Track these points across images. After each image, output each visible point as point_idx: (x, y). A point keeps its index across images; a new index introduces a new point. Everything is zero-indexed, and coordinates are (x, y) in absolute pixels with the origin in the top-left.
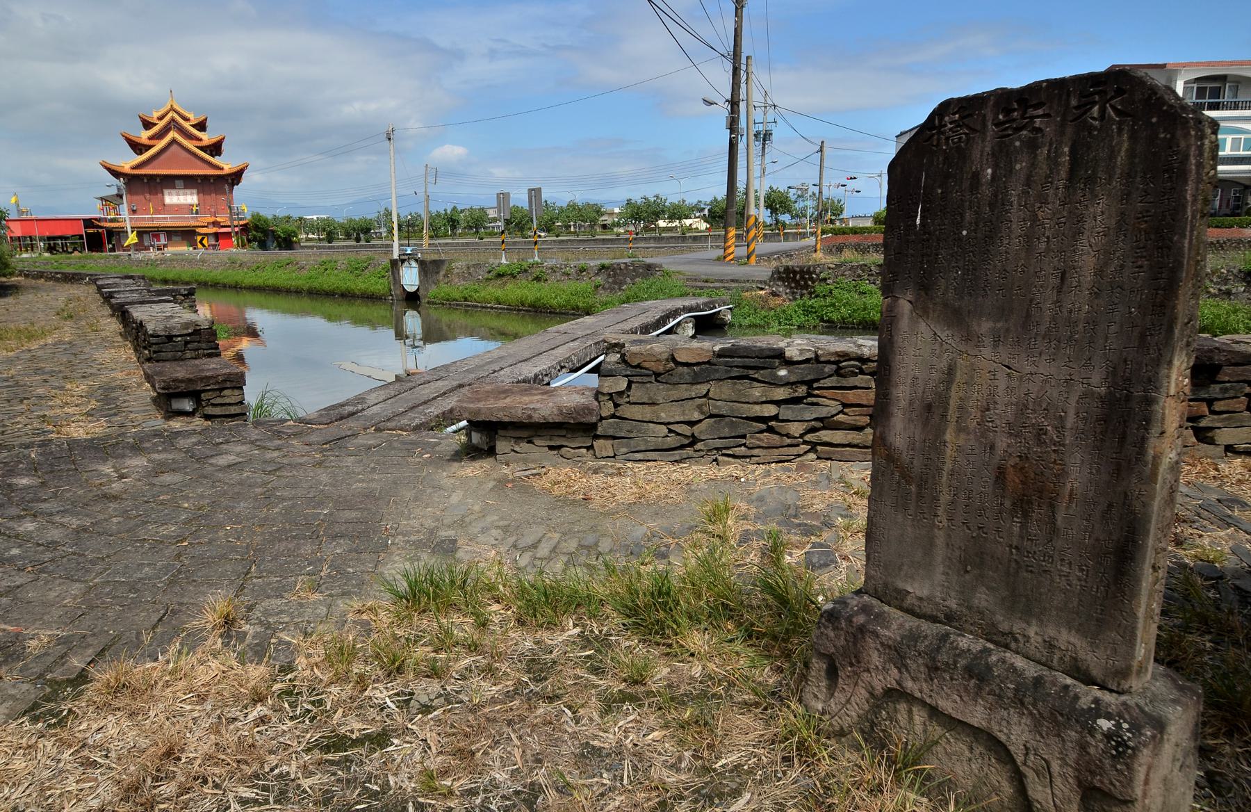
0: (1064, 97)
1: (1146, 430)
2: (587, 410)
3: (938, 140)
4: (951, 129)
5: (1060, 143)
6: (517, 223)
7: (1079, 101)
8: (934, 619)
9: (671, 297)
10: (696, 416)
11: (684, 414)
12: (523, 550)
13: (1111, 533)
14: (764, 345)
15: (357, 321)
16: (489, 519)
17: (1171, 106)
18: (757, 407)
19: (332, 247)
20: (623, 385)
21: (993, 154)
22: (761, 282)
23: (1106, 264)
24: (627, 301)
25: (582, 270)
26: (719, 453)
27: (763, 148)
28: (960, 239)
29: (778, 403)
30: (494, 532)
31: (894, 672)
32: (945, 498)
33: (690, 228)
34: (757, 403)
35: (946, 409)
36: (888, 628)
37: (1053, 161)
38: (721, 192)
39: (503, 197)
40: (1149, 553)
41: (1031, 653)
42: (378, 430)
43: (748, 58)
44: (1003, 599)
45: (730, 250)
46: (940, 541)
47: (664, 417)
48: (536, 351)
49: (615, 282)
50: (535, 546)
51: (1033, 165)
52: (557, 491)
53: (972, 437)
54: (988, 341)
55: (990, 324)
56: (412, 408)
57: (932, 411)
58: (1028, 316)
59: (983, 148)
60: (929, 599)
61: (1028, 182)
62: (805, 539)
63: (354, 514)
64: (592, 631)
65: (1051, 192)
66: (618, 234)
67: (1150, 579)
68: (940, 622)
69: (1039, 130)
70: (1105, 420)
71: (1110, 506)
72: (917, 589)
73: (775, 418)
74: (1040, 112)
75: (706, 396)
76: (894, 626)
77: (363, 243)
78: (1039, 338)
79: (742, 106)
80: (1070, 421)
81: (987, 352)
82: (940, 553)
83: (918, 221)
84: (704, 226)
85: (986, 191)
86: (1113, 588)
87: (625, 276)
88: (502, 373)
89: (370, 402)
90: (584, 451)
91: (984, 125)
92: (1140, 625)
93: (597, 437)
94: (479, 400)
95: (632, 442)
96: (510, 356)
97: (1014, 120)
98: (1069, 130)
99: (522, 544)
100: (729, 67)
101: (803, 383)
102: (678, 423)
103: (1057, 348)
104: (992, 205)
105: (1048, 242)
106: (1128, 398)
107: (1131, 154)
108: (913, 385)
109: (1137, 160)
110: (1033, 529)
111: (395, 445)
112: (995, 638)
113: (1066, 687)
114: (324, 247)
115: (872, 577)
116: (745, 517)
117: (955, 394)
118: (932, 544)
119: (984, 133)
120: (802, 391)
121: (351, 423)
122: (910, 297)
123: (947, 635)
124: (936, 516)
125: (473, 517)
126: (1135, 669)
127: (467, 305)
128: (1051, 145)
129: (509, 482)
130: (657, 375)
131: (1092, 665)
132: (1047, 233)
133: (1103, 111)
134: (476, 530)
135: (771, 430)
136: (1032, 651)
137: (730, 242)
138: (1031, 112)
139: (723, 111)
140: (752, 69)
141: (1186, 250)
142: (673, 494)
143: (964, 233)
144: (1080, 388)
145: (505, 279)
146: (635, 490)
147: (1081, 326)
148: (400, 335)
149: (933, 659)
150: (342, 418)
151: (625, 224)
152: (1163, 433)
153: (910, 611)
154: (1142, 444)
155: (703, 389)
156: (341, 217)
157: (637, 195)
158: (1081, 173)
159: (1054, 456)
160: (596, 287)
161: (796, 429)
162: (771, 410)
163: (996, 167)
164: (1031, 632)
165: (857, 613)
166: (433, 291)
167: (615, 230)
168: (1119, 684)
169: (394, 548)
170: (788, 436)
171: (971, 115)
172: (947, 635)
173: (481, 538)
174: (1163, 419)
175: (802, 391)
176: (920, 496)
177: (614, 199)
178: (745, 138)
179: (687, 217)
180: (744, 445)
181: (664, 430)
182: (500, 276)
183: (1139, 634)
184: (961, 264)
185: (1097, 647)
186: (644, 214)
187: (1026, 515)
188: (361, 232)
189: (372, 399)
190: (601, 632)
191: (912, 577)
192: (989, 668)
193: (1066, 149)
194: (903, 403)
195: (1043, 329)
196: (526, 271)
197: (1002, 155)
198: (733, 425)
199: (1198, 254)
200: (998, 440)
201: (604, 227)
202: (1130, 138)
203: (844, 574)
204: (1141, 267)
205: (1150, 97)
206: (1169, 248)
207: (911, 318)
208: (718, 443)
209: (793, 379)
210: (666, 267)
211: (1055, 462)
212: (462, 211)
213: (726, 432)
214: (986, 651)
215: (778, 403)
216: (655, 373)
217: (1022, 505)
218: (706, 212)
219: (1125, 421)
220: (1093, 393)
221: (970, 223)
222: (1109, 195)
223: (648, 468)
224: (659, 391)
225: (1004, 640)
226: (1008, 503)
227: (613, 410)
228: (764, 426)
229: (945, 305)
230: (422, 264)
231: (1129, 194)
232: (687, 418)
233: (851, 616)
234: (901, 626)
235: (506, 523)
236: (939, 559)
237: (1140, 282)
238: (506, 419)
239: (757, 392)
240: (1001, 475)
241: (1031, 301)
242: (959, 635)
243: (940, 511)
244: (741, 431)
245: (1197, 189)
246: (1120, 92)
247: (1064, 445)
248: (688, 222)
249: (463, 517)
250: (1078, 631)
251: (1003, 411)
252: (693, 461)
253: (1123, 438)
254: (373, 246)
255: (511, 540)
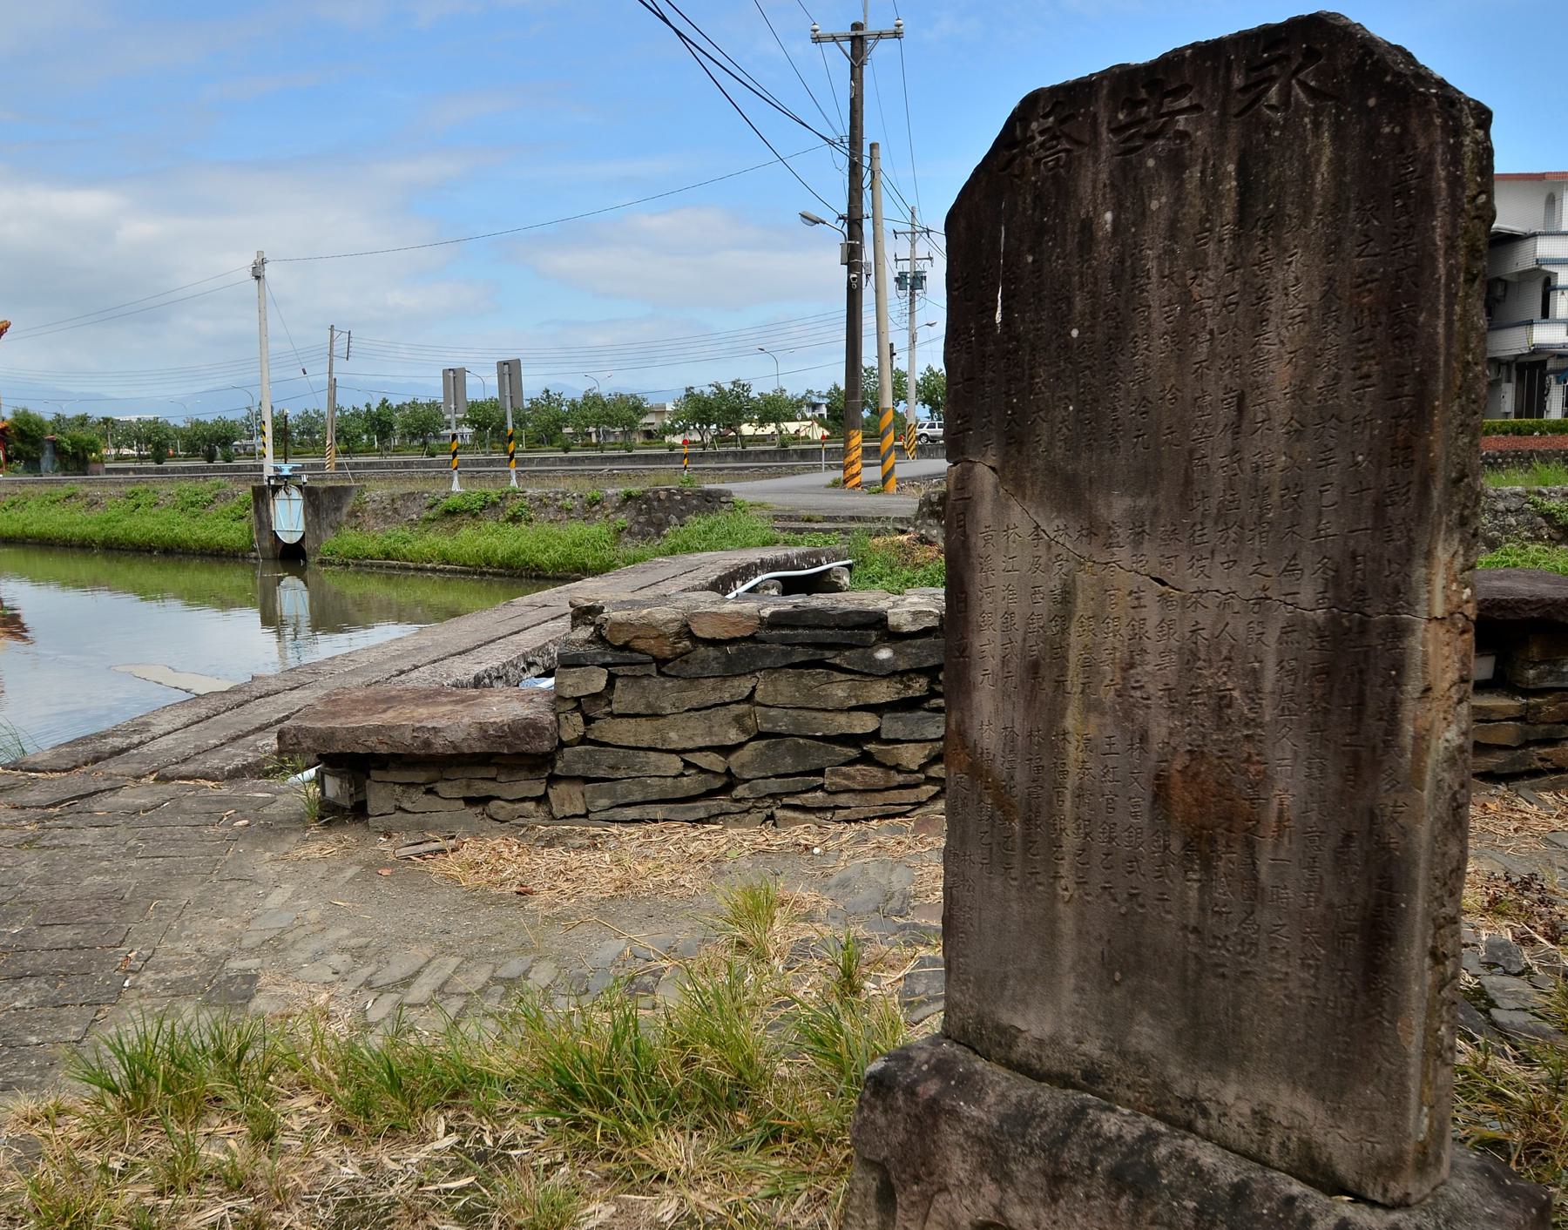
0: (1222, 73)
1: (1398, 685)
2: (530, 728)
3: (1023, 164)
4: (1042, 145)
5: (1221, 156)
6: (489, 424)
7: (1247, 76)
8: (1063, 1081)
9: (746, 546)
10: (733, 736)
11: (710, 734)
12: (382, 991)
13: (1352, 892)
14: (851, 607)
15: (195, 598)
16: (332, 935)
17: (1398, 75)
18: (842, 719)
19: (164, 471)
20: (599, 681)
21: (1112, 184)
22: (901, 520)
23: (1310, 376)
24: (673, 551)
25: (594, 502)
26: (773, 806)
27: (912, 302)
28: (1067, 344)
29: (877, 709)
30: (337, 960)
31: (990, 1190)
32: (1070, 841)
33: (796, 437)
34: (840, 711)
35: (1063, 669)
36: (978, 1102)
37: (1211, 189)
38: (836, 376)
39: (455, 378)
40: (1419, 926)
41: (1231, 1136)
42: (163, 779)
43: (873, 146)
44: (1179, 1033)
45: (854, 469)
46: (1067, 927)
47: (675, 738)
48: (485, 637)
49: (650, 523)
50: (406, 982)
51: (1179, 200)
52: (470, 880)
53: (1108, 720)
54: (1123, 533)
55: (1127, 502)
56: (234, 739)
57: (1039, 674)
58: (1188, 482)
59: (1094, 176)
60: (1055, 1041)
61: (1173, 230)
62: (909, 952)
63: (69, 934)
64: (480, 1141)
65: (1211, 247)
66: (672, 447)
67: (1429, 978)
68: (1075, 1086)
69: (1184, 135)
70: (1326, 672)
71: (1348, 837)
72: (1033, 1023)
73: (875, 736)
74: (1185, 102)
75: (749, 699)
76: (991, 1098)
77: (219, 463)
78: (1209, 523)
79: (867, 226)
80: (1269, 680)
81: (1123, 554)
82: (1068, 952)
83: (998, 318)
84: (818, 433)
85: (1105, 254)
86: (1363, 998)
87: (668, 511)
88: (414, 674)
89: (156, 730)
90: (531, 806)
91: (1096, 134)
92: (1414, 1070)
93: (553, 780)
94: (334, 715)
95: (619, 787)
96: (436, 645)
97: (1144, 120)
98: (1234, 132)
99: (379, 981)
100: (844, 162)
101: (920, 672)
102: (700, 749)
103: (1240, 540)
104: (1116, 279)
105: (1212, 339)
106: (1364, 627)
107: (1338, 166)
108: (1006, 629)
109: (1348, 178)
110: (1221, 892)
111: (187, 804)
112: (1169, 1110)
113: (1290, 1200)
114: (147, 471)
115: (957, 1005)
116: (809, 917)
117: (1076, 641)
118: (1054, 934)
119: (1096, 148)
120: (919, 686)
121: (114, 767)
122: (992, 460)
123: (1083, 1109)
124: (1057, 877)
125: (302, 932)
126: (1410, 1158)
127: (391, 565)
128: (1205, 161)
129: (385, 866)
130: (661, 662)
131: (1336, 1154)
132: (1210, 325)
133: (1286, 93)
134: (301, 957)
135: (867, 759)
136: (1233, 1133)
137: (854, 456)
138: (1169, 105)
139: (836, 235)
140: (883, 163)
141: (1441, 339)
142: (684, 880)
143: (1075, 333)
144: (1283, 614)
145: (458, 520)
146: (617, 873)
147: (1275, 497)
148: (270, 619)
149: (1055, 1159)
150: (96, 760)
151: (684, 430)
152: (1428, 690)
153: (1024, 1069)
154: (1391, 715)
155: (743, 686)
156: (178, 419)
157: (707, 377)
158: (1257, 216)
159: (1247, 748)
160: (619, 532)
161: (912, 756)
162: (865, 723)
163: (1118, 208)
164: (1229, 1094)
165: (926, 1077)
166: (330, 541)
167: (667, 439)
168: (1386, 1190)
169: (133, 994)
170: (898, 768)
171: (1072, 116)
172: (1083, 1109)
173: (308, 970)
174: (1425, 663)
175: (919, 686)
176: (1028, 842)
177: (663, 384)
178: (872, 278)
179: (792, 419)
180: (821, 787)
181: (676, 764)
182: (451, 513)
183: (1413, 1086)
184: (1072, 391)
185: (1344, 1118)
186: (718, 411)
187: (1207, 866)
188: (214, 443)
189: (162, 724)
190: (496, 1140)
191: (1024, 1002)
192: (1153, 1171)
193: (1231, 168)
194: (992, 664)
195: (1213, 503)
196: (494, 504)
197: (1127, 186)
198: (798, 752)
199: (1467, 350)
200: (1152, 725)
201: (649, 434)
202: (1334, 138)
203: (903, 1005)
204: (1368, 376)
205: (1362, 61)
206: (1413, 336)
207: (996, 501)
208: (774, 785)
209: (902, 665)
210: (737, 497)
211: (1248, 760)
212: (399, 408)
213: (788, 764)
214: (1151, 1137)
215: (877, 709)
216: (655, 659)
217: (1200, 848)
218: (824, 410)
219: (1361, 672)
220: (1304, 621)
221: (1082, 315)
222: (1306, 247)
223: (648, 835)
224: (666, 694)
225: (1186, 1116)
226: (1176, 846)
227: (581, 729)
228: (853, 753)
229: (1052, 470)
230: (309, 494)
231: (1339, 242)
232: (716, 741)
233: (915, 1082)
234: (1003, 1097)
235: (363, 941)
236: (1067, 962)
237: (1368, 405)
238: (384, 750)
239: (839, 691)
240: (1161, 789)
241: (1191, 452)
242: (1104, 1109)
243: (1065, 868)
244: (814, 762)
245: (1454, 226)
246: (1311, 55)
247: (1260, 725)
248: (792, 427)
249: (283, 931)
250: (1309, 1087)
251: (1157, 670)
252: (730, 819)
253: (1361, 703)
254: (238, 469)
255: (364, 973)
